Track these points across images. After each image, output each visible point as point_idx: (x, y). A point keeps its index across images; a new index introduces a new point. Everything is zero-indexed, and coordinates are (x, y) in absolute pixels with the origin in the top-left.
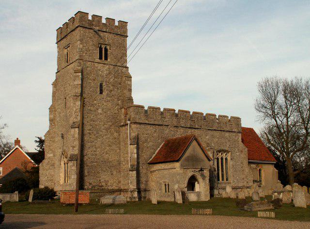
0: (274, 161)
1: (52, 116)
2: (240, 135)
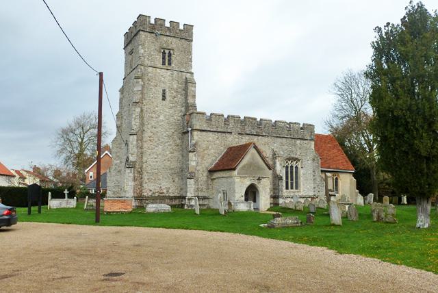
1: (119, 123)
2: (313, 143)
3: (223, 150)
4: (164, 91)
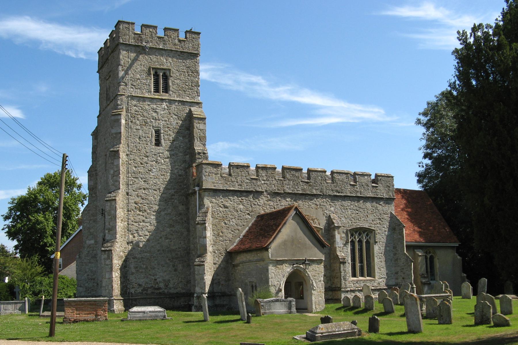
0: (455, 242)
3: (251, 220)
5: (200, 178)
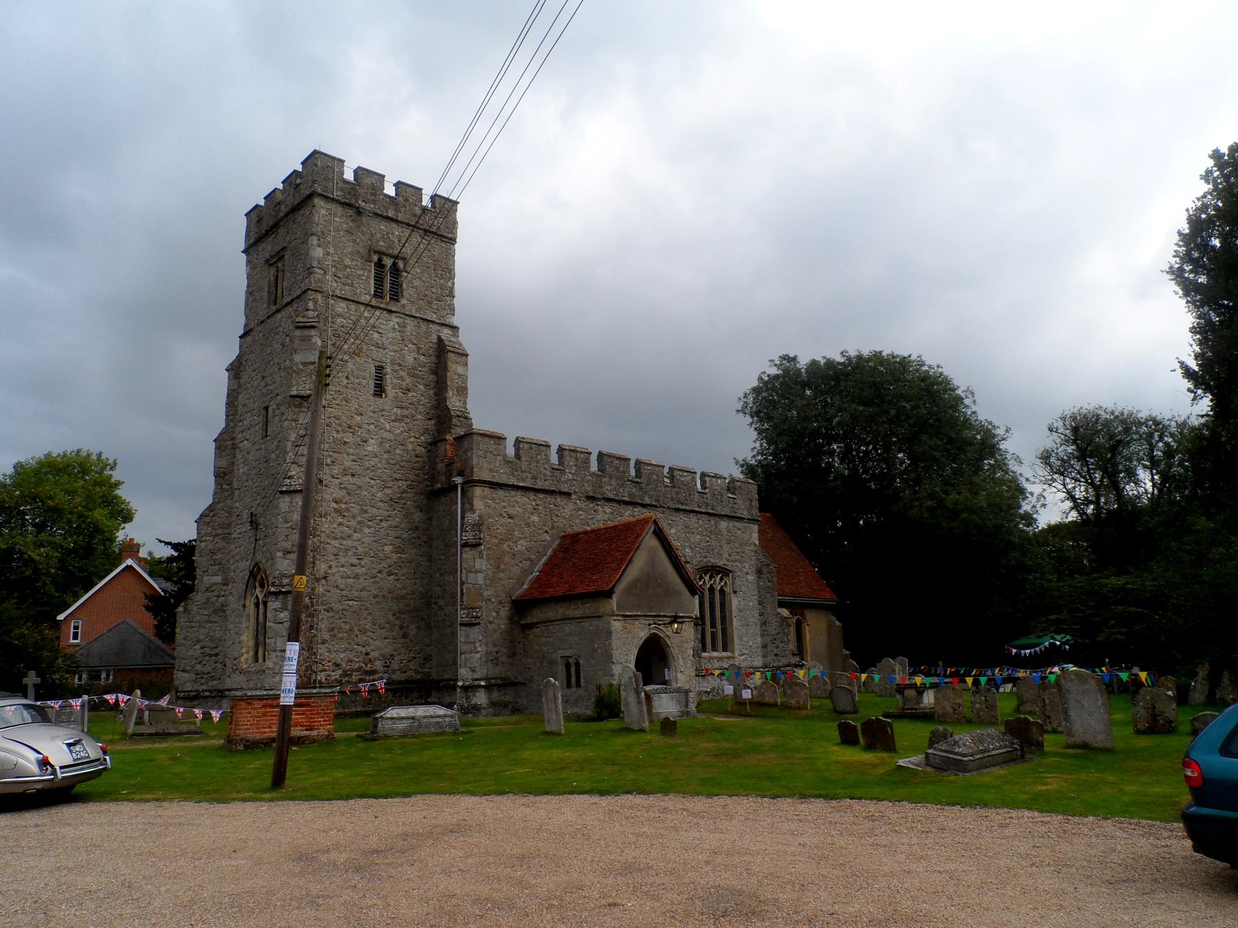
2: (755, 528)
4: (380, 369)
5: (466, 460)
